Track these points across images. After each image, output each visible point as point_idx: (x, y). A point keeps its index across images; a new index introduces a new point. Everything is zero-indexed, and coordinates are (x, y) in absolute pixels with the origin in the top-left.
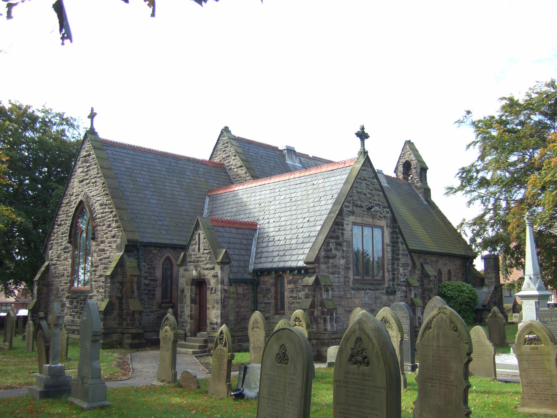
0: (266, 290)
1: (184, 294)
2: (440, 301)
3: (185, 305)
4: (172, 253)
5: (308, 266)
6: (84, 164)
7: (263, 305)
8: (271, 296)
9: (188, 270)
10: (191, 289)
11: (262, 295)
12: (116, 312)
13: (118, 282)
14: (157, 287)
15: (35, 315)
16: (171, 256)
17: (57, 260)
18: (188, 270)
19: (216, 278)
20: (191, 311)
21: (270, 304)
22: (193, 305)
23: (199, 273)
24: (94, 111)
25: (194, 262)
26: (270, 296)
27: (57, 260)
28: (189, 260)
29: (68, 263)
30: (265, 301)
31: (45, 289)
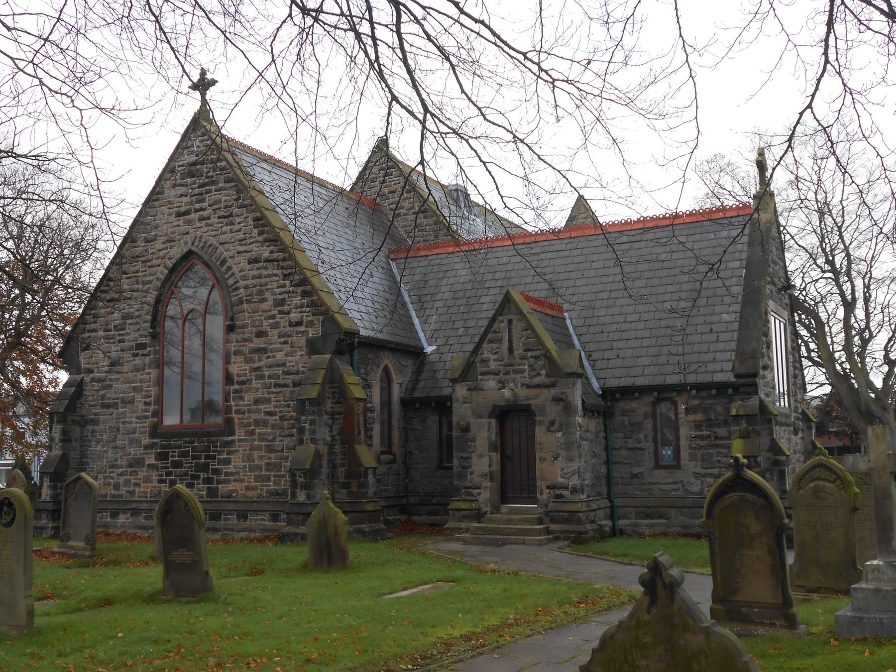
0: (631, 425)
1: (471, 435)
2: (23, 481)
3: (473, 454)
4: (391, 358)
5: (741, 381)
6: (189, 180)
7: (624, 453)
8: (646, 436)
9: (482, 390)
10: (489, 423)
11: (621, 435)
12: (325, 470)
13: (326, 413)
14: (374, 423)
15: (59, 485)
16: (390, 365)
17: (106, 372)
18: (482, 390)
19: (562, 404)
20: (490, 466)
21: (644, 449)
22: (494, 454)
23: (515, 395)
24: (209, 76)
25: (497, 374)
26: (642, 436)
27: (106, 372)
28: (480, 369)
29: (148, 377)
30: (630, 445)
31: (76, 432)
